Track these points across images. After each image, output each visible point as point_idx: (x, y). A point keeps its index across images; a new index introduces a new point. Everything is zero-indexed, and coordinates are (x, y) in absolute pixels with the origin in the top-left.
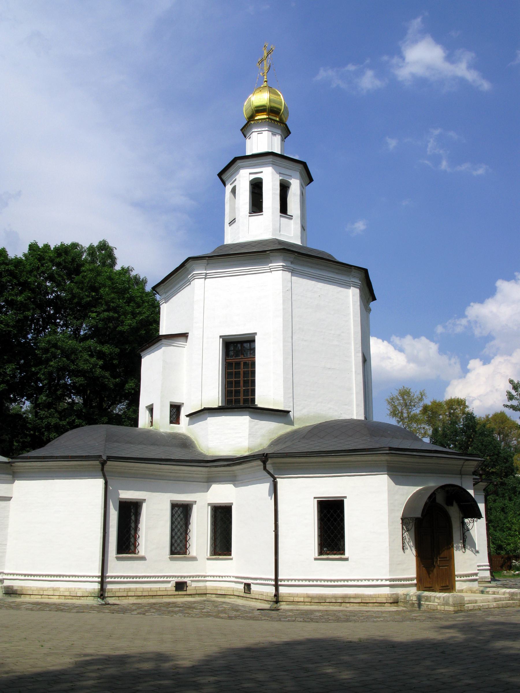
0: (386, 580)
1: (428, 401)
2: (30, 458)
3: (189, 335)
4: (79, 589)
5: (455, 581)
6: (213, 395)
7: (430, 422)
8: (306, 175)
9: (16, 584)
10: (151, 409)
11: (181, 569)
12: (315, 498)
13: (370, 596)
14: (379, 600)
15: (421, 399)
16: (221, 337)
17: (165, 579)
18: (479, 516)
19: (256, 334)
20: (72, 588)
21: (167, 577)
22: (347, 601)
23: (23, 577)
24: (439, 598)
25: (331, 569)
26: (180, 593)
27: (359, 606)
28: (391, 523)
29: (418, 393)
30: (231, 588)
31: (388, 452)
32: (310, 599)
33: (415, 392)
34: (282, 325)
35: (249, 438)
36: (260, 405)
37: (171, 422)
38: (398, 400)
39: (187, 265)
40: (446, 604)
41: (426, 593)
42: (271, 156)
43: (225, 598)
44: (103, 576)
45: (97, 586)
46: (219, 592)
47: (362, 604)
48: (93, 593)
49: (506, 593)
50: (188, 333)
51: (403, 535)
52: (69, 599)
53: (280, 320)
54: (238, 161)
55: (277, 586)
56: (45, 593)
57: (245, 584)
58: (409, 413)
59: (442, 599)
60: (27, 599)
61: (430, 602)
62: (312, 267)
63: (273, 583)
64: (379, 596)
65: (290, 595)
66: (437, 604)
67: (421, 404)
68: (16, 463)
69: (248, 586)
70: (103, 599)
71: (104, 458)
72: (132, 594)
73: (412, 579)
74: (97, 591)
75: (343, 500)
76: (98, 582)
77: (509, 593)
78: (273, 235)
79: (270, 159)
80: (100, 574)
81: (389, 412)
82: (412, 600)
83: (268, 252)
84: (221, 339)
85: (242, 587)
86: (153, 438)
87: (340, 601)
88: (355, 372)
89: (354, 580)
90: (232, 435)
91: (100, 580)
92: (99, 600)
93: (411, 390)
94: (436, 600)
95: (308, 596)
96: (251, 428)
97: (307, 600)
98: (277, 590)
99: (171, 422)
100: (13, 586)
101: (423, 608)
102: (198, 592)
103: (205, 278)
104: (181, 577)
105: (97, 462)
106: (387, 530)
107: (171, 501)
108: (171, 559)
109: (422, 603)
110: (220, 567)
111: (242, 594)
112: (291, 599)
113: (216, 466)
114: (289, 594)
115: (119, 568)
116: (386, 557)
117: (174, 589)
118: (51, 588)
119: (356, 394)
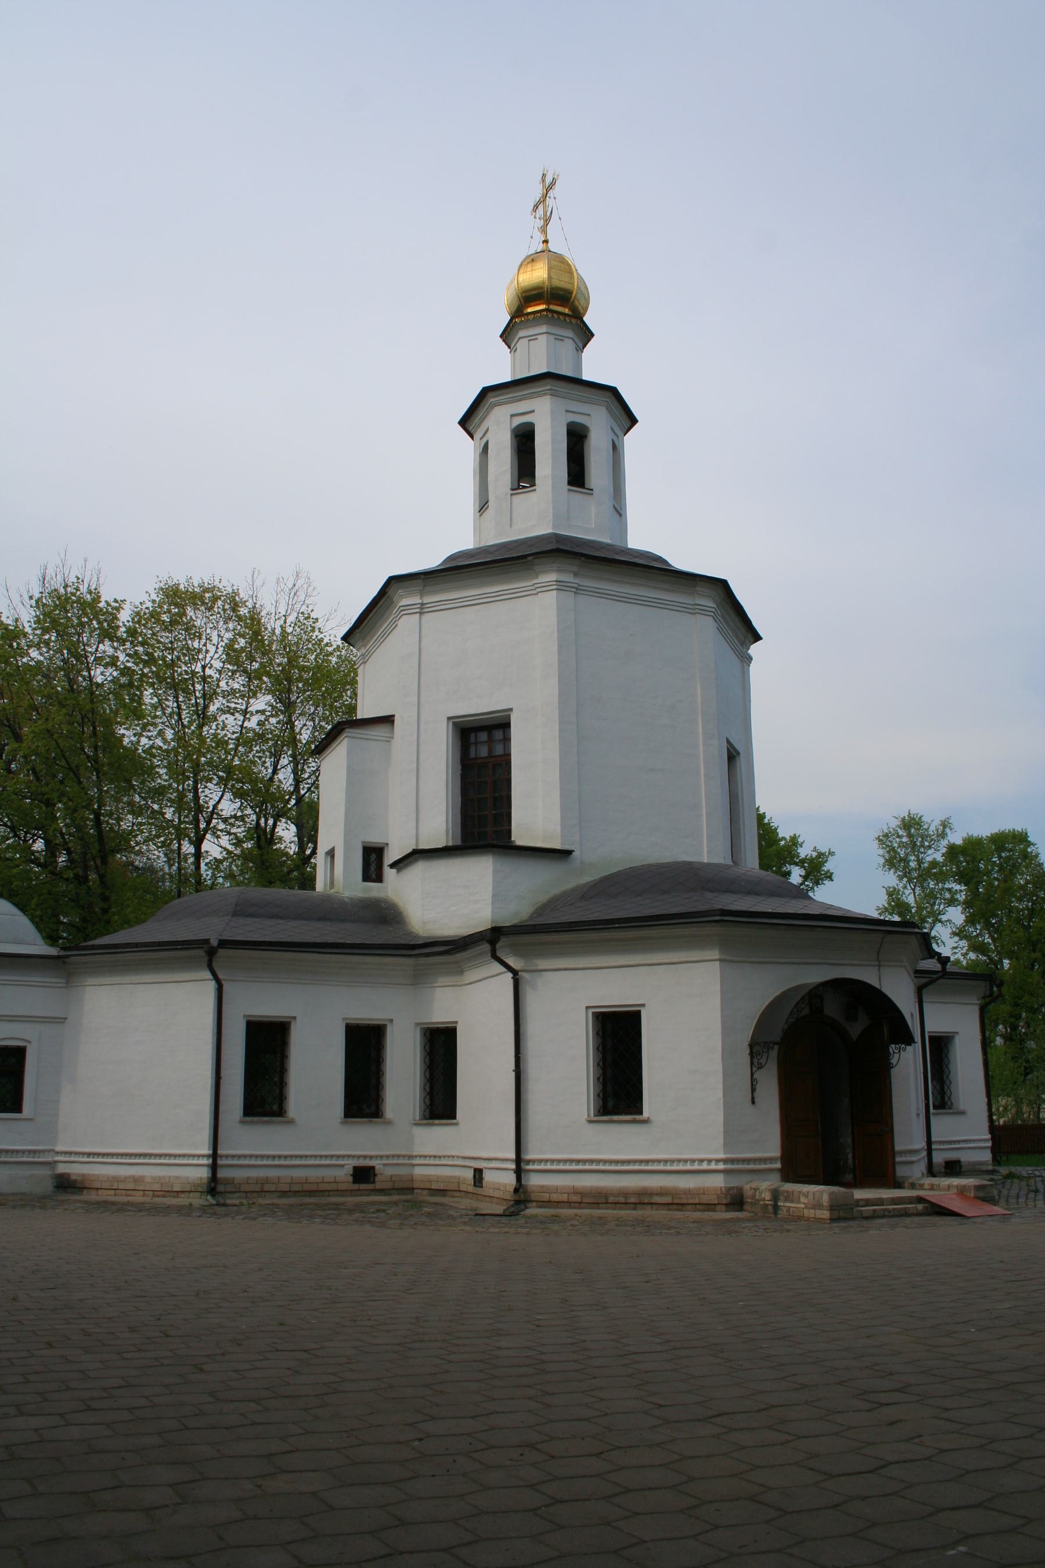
0: (718, 1161)
1: (956, 838)
2: (93, 947)
3: (397, 720)
4: (178, 1178)
5: (894, 1163)
6: (437, 825)
7: (963, 877)
8: (622, 412)
9: (76, 1170)
10: (331, 854)
11: (363, 1142)
12: (587, 1008)
13: (688, 1192)
14: (705, 1199)
15: (943, 835)
16: (449, 718)
17: (334, 1162)
18: (909, 1040)
19: (511, 710)
20: (164, 1177)
21: (338, 1157)
22: (646, 1201)
23: (86, 1159)
24: (806, 1195)
25: (619, 1141)
26: (363, 1186)
27: (669, 1210)
28: (727, 1053)
29: (937, 823)
30: (455, 1177)
31: (718, 918)
32: (579, 1196)
33: (932, 821)
34: (556, 691)
35: (493, 902)
36: (520, 842)
37: (366, 878)
38: (899, 836)
39: (390, 592)
40: (818, 1206)
41: (789, 1187)
42: (548, 381)
43: (444, 1196)
44: (215, 1155)
45: (204, 1173)
46: (434, 1186)
47: (675, 1207)
48: (199, 1185)
49: (953, 1186)
50: (393, 716)
51: (752, 1075)
52: (158, 1196)
53: (554, 682)
54: (490, 394)
55: (519, 1172)
56: (121, 1186)
57: (475, 1170)
58: (920, 862)
59: (811, 1196)
60: (93, 1196)
61: (792, 1202)
62: (616, 581)
63: (513, 1166)
64: (704, 1191)
65: (544, 1189)
66: (803, 1206)
67: (944, 843)
68: (72, 958)
69: (478, 1173)
70: (213, 1196)
71: (214, 943)
72: (272, 1188)
73: (771, 1160)
74: (206, 1181)
75: (639, 1012)
76: (207, 1165)
77: (957, 1186)
78: (554, 527)
79: (547, 385)
80: (211, 1152)
81: (882, 861)
82: (764, 1200)
83: (529, 558)
84: (451, 724)
85: (469, 1174)
86: (332, 910)
87: (633, 1200)
88: (705, 775)
89: (659, 1161)
90: (453, 898)
91: (210, 1161)
92: (209, 1197)
93: (923, 819)
94: (802, 1199)
95: (575, 1191)
96: (496, 884)
97: (575, 1198)
98: (519, 1179)
99: (366, 878)
100: (69, 1175)
101: (783, 1213)
102: (397, 1186)
103: (421, 613)
104: (365, 1157)
105: (201, 953)
106: (721, 1067)
107: (245, 1016)
108: (242, 1122)
109: (780, 1204)
110: (434, 1139)
111: (471, 1189)
112: (546, 1197)
113: (427, 955)
114: (542, 1187)
115: (254, 1144)
116: (718, 1118)
117: (351, 1179)
118: (130, 1177)
119: (707, 814)
